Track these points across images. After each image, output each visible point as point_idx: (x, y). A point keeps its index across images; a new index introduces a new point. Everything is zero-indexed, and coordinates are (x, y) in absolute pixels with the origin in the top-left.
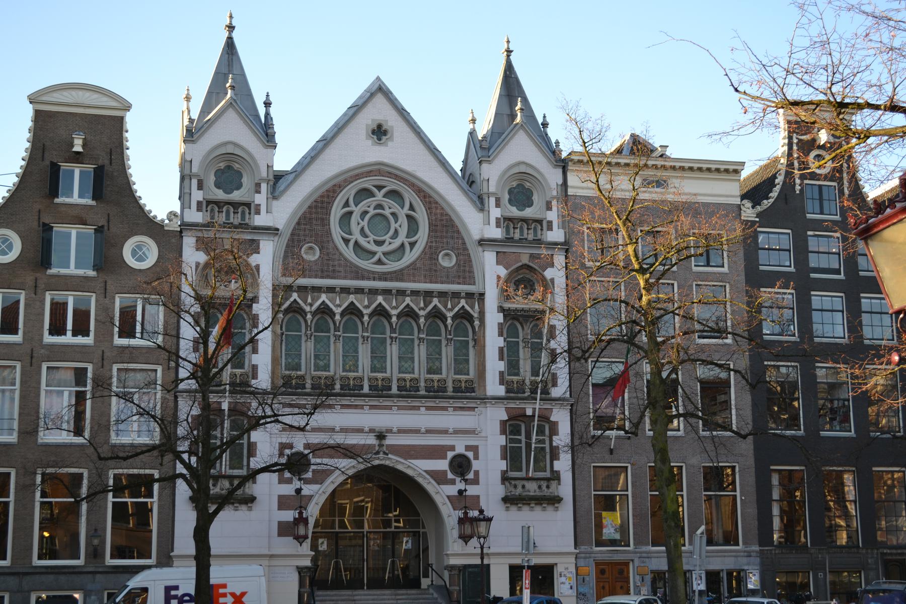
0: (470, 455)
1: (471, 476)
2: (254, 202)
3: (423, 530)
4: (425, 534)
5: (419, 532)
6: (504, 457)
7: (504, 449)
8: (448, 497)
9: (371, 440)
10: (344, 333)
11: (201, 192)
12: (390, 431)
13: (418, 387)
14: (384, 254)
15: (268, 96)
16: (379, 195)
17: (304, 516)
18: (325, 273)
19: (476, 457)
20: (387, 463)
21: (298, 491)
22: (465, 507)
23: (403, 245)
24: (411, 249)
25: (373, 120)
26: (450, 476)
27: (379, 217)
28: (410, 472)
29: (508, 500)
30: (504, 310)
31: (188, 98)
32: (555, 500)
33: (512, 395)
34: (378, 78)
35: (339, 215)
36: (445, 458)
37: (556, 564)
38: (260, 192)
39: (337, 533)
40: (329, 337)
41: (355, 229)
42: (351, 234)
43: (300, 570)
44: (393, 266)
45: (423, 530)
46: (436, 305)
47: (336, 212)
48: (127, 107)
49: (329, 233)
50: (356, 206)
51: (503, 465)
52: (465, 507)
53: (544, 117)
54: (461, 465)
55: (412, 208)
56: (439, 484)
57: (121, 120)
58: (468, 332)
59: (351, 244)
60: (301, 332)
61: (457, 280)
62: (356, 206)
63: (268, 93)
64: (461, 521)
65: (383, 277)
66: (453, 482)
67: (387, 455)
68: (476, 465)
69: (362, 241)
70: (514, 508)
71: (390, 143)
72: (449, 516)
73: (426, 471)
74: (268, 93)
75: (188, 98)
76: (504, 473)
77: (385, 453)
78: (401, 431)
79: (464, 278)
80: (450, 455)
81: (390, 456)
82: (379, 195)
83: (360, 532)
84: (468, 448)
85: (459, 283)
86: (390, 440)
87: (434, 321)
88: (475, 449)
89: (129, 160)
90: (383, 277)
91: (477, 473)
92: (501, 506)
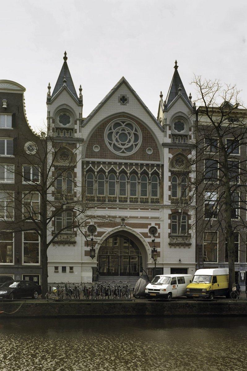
0: (157, 227)
4: (141, 256)
6: (170, 228)
7: (170, 225)
19: (159, 228)
22: (154, 246)
26: (149, 235)
27: (122, 134)
29: (171, 245)
31: (161, 96)
32: (189, 245)
35: (107, 133)
36: (147, 228)
37: (188, 268)
43: (93, 268)
47: (106, 132)
48: (24, 89)
51: (169, 231)
53: (190, 94)
54: (153, 231)
57: (22, 95)
65: (124, 158)
68: (159, 231)
70: (173, 247)
72: (148, 250)
75: (161, 96)
76: (169, 234)
80: (149, 227)
82: (123, 125)
84: (156, 224)
88: (159, 225)
89: (25, 111)
91: (159, 234)
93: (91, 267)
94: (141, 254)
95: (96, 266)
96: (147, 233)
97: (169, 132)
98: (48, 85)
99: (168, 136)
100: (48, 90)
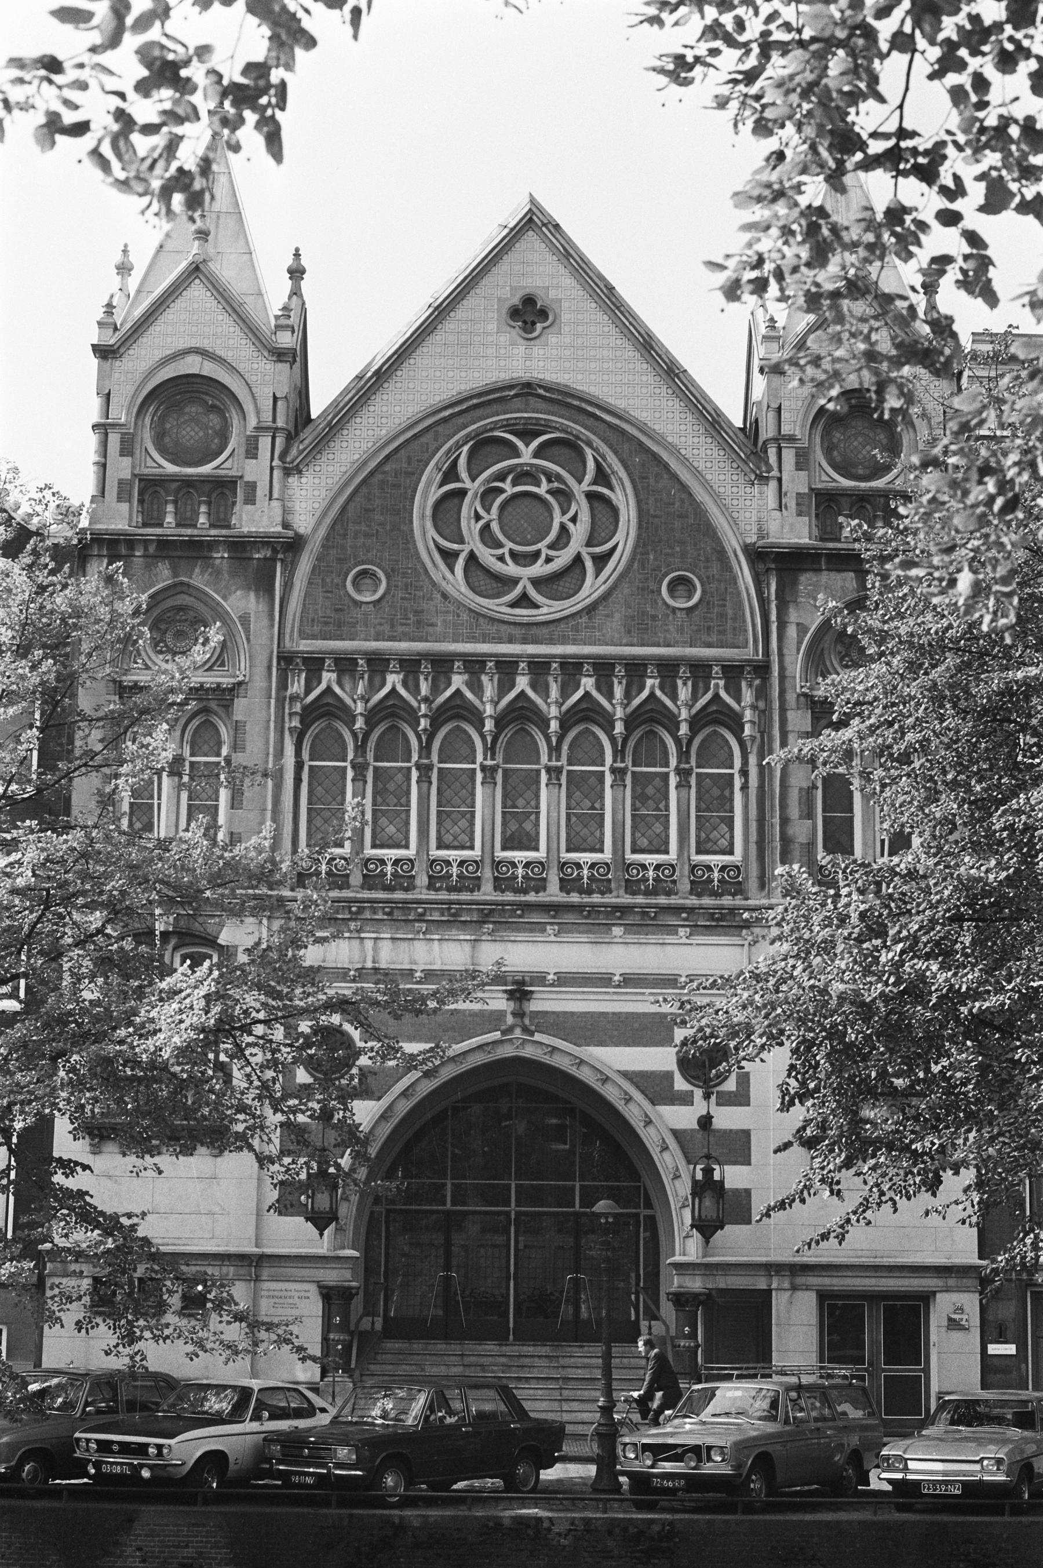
1: (730, 1085)
2: (241, 477)
3: (649, 1212)
5: (637, 1215)
8: (675, 1133)
9: (498, 1002)
10: (506, 762)
11: (127, 461)
12: (540, 979)
13: (479, 878)
14: (536, 582)
15: (297, 255)
16: (527, 453)
17: (717, 1176)
18: (400, 629)
20: (528, 1052)
21: (705, 1122)
22: (708, 1157)
23: (578, 559)
24: (598, 573)
25: (513, 289)
26: (680, 1084)
28: (586, 1075)
30: (814, 703)
31: (124, 269)
33: (575, 898)
34: (533, 201)
36: (668, 1041)
38: (255, 457)
39: (448, 1213)
40: (667, 774)
41: (470, 529)
42: (462, 541)
44: (549, 609)
45: (649, 1212)
46: (523, 692)
49: (408, 537)
50: (473, 480)
52: (708, 1157)
55: (602, 477)
56: (653, 1104)
58: (731, 755)
59: (460, 565)
60: (731, 767)
61: (705, 638)
62: (473, 480)
63: (297, 250)
64: (699, 1189)
65: (529, 632)
66: (686, 1099)
67: (532, 1035)
69: (487, 556)
71: (552, 339)
73: (625, 1075)
74: (297, 250)
77: (525, 1030)
78: (565, 980)
79: (721, 632)
81: (537, 1037)
82: (527, 453)
83: (499, 1213)
85: (709, 645)
86: (543, 1002)
87: (652, 732)
90: (529, 632)
92: (91, 1156)
93: (313, 1288)
94: (649, 1205)
95: (332, 1276)
96: (668, 1076)
97: (796, 482)
98: (289, 261)
99: (791, 502)
100: (289, 283)
